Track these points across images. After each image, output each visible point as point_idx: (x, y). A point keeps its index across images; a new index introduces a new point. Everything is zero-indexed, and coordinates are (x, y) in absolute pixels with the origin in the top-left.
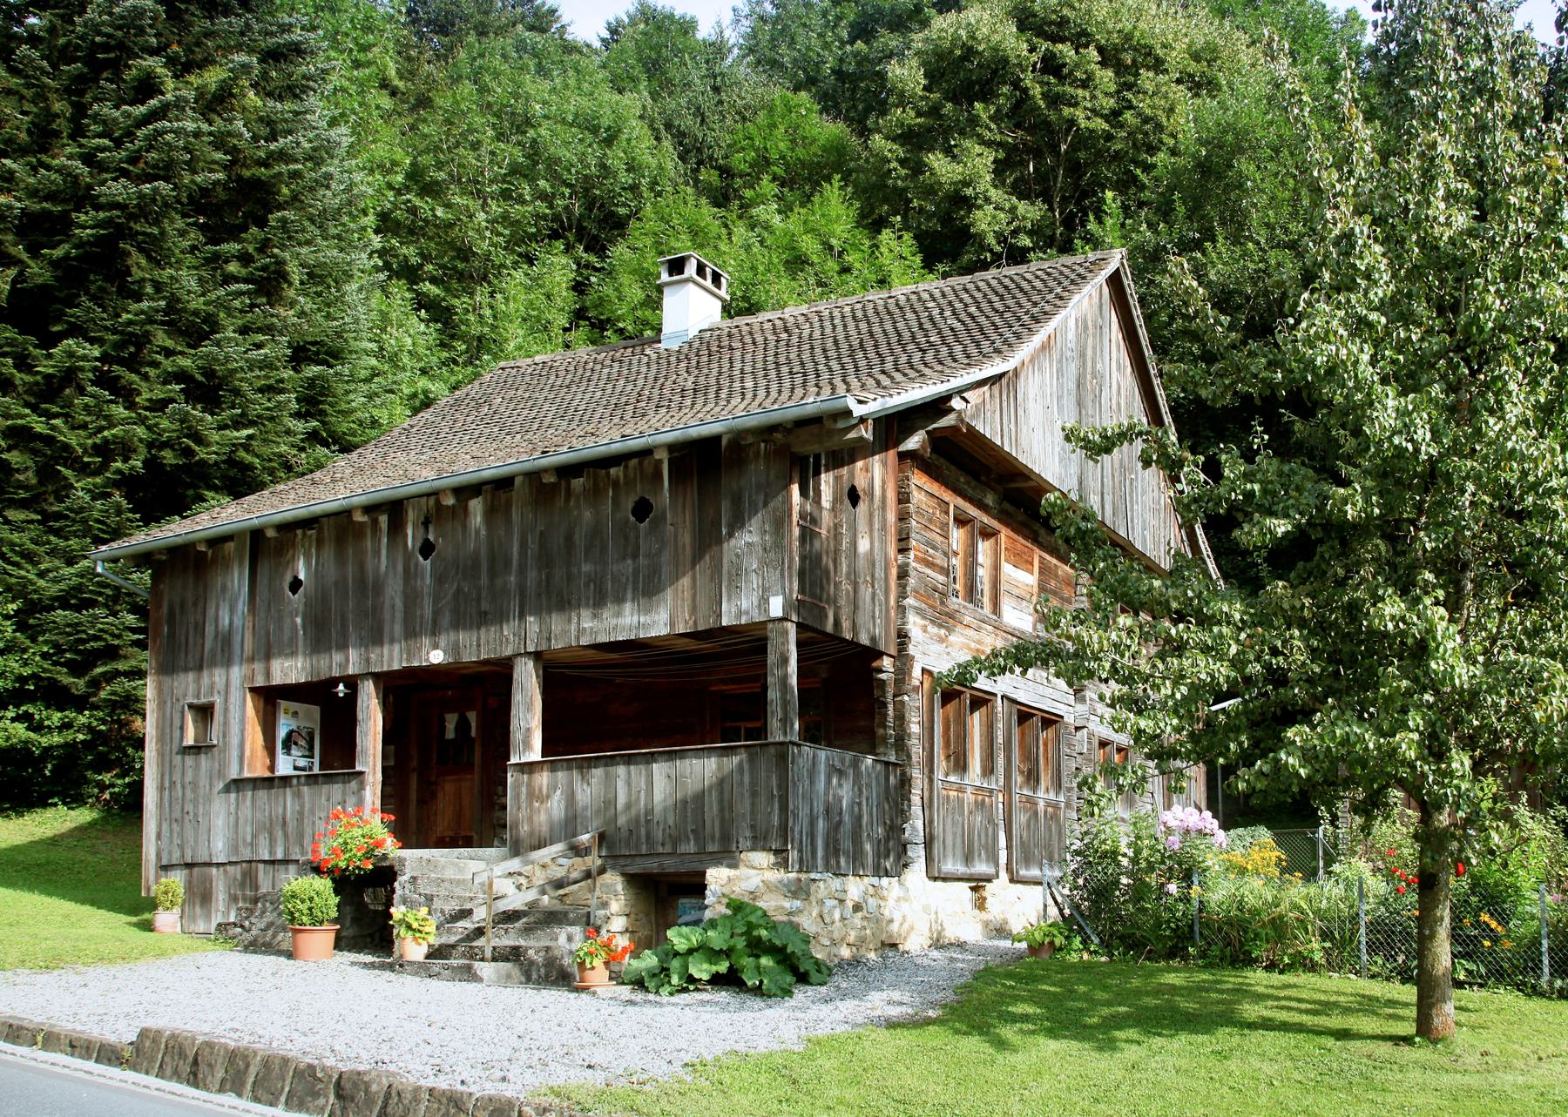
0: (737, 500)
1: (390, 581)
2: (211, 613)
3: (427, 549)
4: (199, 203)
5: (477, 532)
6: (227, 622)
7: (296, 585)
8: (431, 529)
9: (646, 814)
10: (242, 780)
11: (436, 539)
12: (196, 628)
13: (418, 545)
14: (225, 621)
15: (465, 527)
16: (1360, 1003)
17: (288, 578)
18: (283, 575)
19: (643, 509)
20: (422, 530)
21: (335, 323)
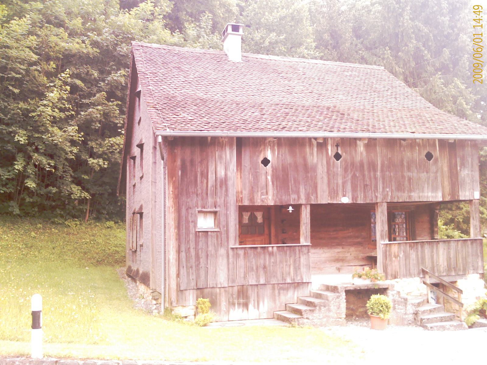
0: (463, 159)
1: (320, 166)
2: (211, 168)
3: (338, 156)
4: (129, 269)
5: (361, 153)
6: (223, 173)
7: (266, 162)
8: (339, 148)
9: (372, 267)
10: (476, 240)
11: (342, 153)
12: (202, 174)
13: (334, 154)
14: (221, 173)
15: (356, 151)
16: (189, 267)
17: (261, 158)
18: (258, 156)
19: (429, 156)
20: (336, 148)
21: (304, 20)
